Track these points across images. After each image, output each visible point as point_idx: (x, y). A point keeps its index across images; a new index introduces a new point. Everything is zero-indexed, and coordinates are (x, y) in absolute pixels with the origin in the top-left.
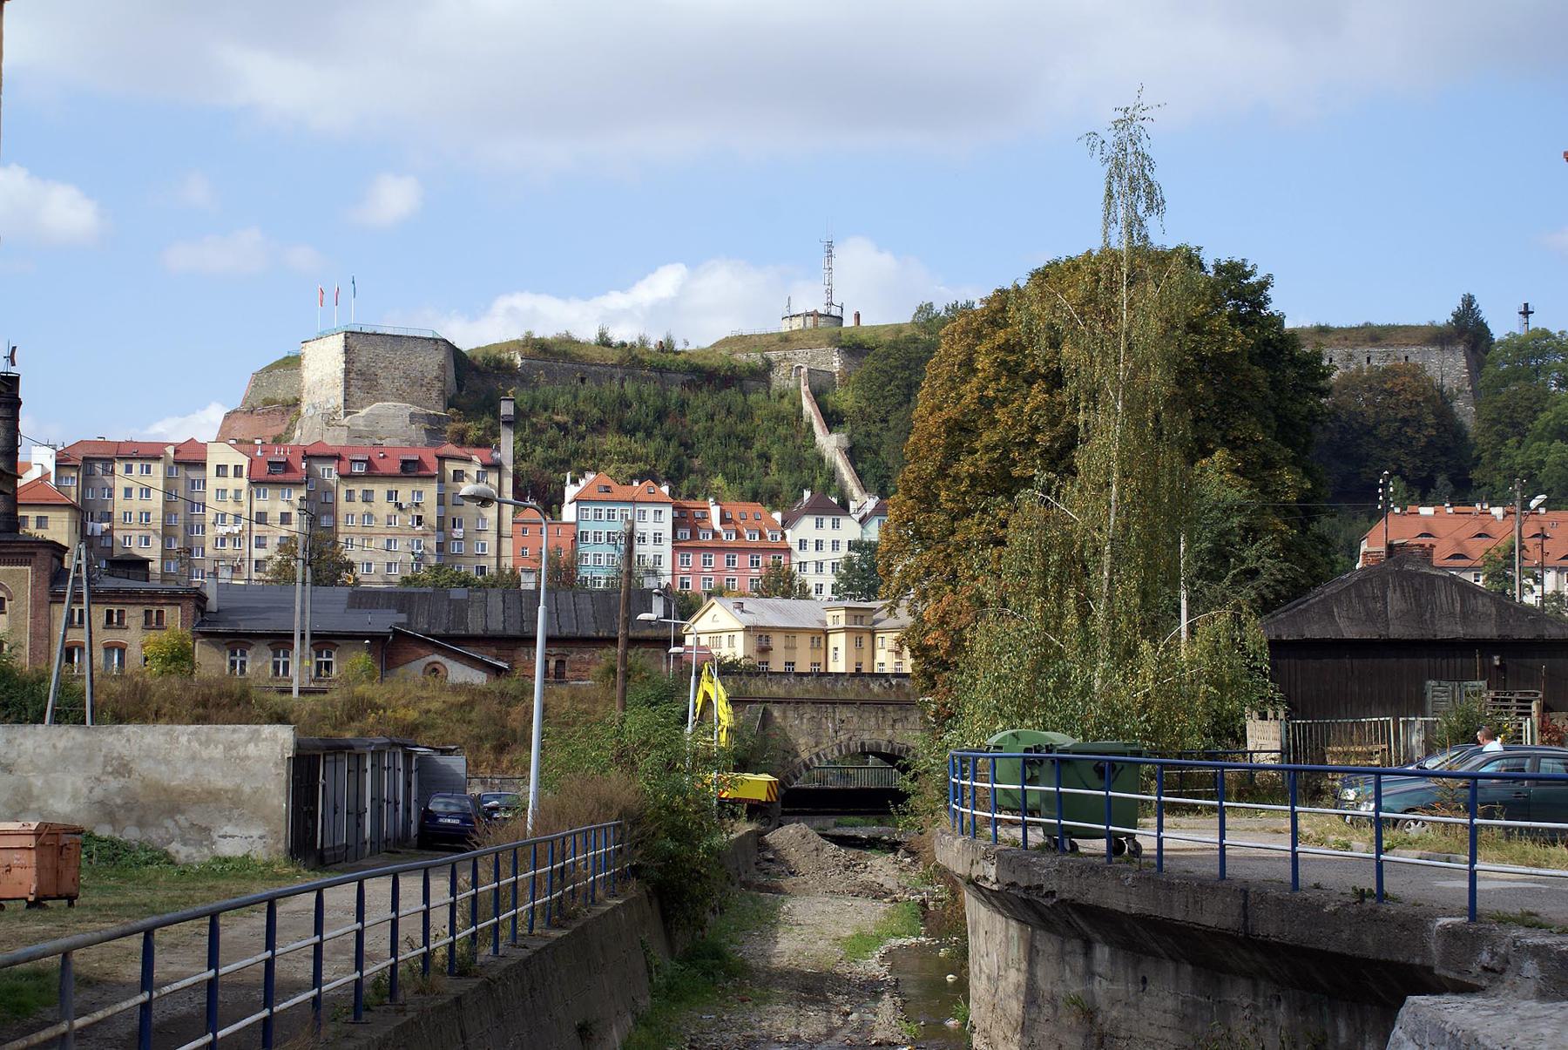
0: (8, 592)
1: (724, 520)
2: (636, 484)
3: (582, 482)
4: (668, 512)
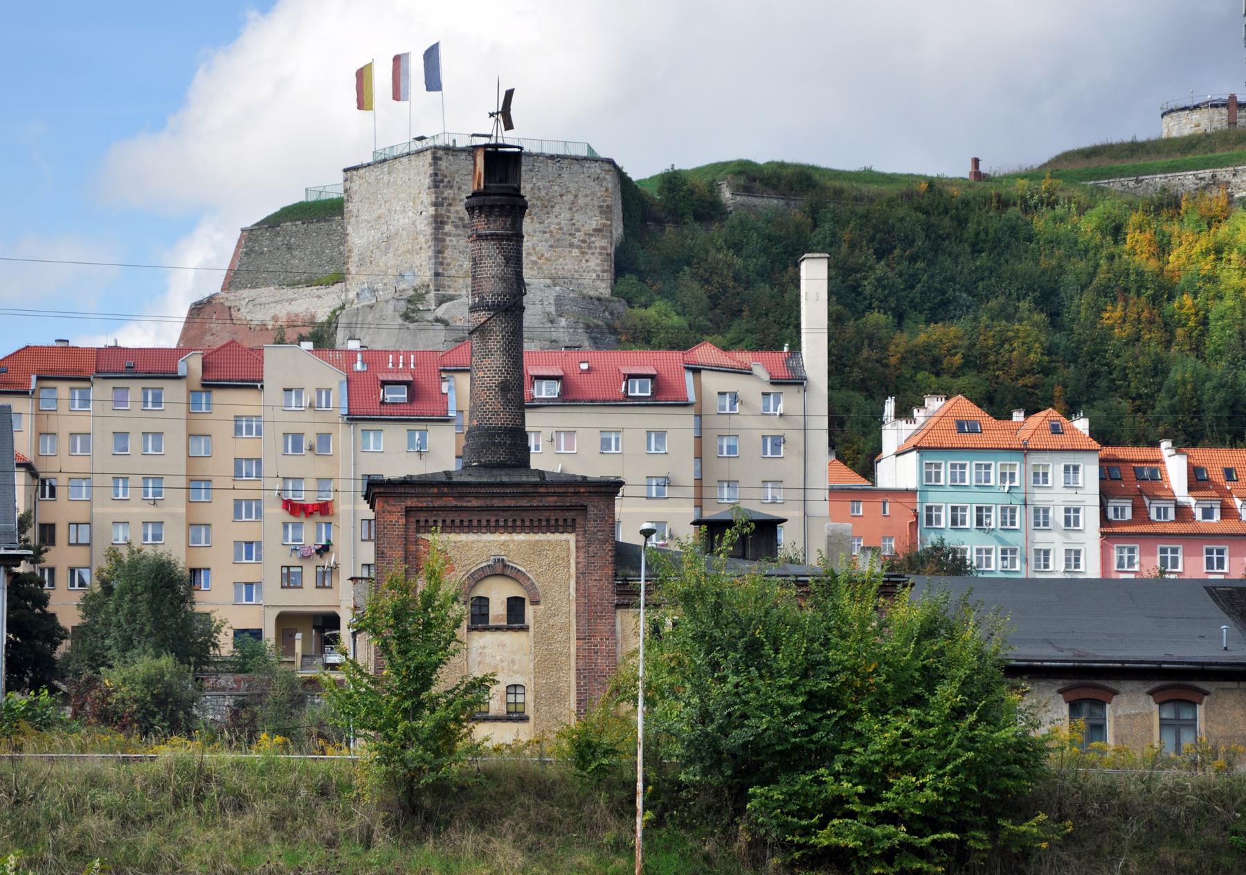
0: (531, 588)
1: (1197, 480)
2: (1018, 416)
3: (919, 415)
4: (1090, 474)
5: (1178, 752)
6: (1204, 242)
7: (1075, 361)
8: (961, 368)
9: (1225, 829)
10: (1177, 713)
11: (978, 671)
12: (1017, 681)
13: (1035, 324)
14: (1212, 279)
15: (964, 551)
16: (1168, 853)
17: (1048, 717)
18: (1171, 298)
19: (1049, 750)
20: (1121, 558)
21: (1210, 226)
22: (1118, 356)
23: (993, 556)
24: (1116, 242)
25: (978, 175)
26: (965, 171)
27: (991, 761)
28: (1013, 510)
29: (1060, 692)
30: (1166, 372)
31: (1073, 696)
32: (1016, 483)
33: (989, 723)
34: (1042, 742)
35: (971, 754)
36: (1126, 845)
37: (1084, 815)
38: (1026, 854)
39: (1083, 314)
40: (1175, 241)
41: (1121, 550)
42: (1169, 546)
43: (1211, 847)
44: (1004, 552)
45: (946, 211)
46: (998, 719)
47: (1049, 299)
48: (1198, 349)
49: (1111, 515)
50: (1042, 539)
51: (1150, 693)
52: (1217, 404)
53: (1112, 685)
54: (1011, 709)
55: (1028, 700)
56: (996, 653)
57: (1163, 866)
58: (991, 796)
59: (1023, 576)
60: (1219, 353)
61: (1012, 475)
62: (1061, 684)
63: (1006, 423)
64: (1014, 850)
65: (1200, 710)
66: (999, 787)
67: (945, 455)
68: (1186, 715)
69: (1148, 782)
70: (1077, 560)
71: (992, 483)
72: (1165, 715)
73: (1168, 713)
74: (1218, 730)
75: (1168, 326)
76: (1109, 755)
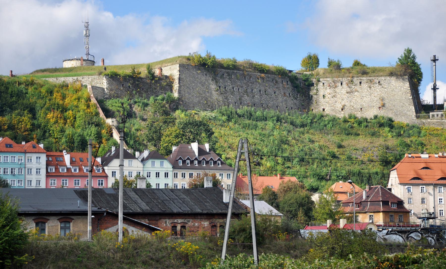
2: (23, 143)
4: (43, 158)
5: (65, 236)
6: (75, 96)
7: (40, 128)
8: (7, 129)
9: (76, 256)
10: (65, 225)
11: (10, 215)
12: (21, 217)
13: (29, 117)
14: (77, 107)
15: (7, 181)
16: (61, 263)
17: (30, 227)
18: (66, 111)
19: (29, 236)
20: (52, 183)
21: (76, 92)
22: (51, 127)
23: (15, 182)
24: (51, 95)
25: (12, 75)
26: (9, 74)
27: (13, 240)
28: (22, 169)
29: (33, 220)
30: (65, 131)
31: (37, 221)
32: (23, 162)
33: (13, 229)
34: (27, 234)
35: (7, 238)
36: (49, 262)
37: (38, 254)
38: (21, 265)
39: (42, 115)
40: (67, 96)
41: (52, 180)
42: (65, 179)
43: (73, 261)
44: (19, 181)
45: (3, 85)
46: (15, 228)
47: (32, 111)
48: (73, 126)
49: (49, 171)
50: (28, 177)
51: (58, 220)
52: (78, 140)
53: (48, 218)
54: (19, 225)
55: (24, 222)
56: (15, 210)
57: (59, 267)
58: (12, 250)
59: (23, 188)
60: (79, 126)
61: (22, 159)
62: (33, 218)
63: (20, 145)
64: (18, 265)
65: (71, 224)
66: (16, 246)
67: (2, 154)
68: (68, 225)
69: (56, 244)
70: (39, 183)
71: (16, 161)
72: (62, 226)
73: (63, 225)
74: (76, 229)
75: (65, 119)
76: (46, 236)
